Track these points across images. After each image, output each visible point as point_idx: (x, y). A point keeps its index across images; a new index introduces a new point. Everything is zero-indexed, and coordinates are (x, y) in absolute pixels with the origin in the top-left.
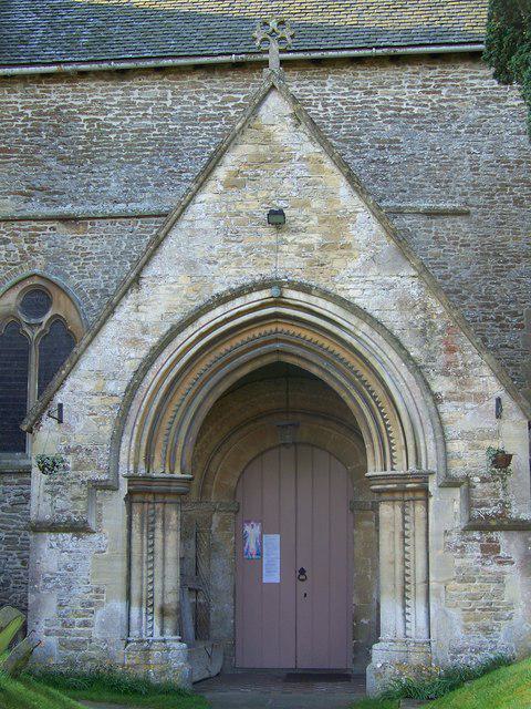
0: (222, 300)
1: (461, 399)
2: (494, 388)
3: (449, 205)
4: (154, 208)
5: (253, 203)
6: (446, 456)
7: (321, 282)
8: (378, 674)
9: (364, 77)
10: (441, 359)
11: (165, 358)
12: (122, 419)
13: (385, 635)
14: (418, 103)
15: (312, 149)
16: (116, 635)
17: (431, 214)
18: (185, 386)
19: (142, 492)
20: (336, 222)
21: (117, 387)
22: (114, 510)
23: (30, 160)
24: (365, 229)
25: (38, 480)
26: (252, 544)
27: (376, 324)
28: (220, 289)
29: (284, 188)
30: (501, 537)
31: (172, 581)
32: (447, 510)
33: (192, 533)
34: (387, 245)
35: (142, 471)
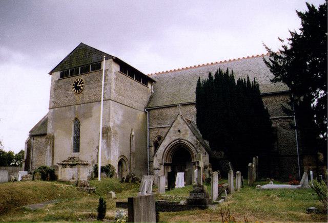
11: (167, 148)
12: (163, 156)
27: (191, 143)
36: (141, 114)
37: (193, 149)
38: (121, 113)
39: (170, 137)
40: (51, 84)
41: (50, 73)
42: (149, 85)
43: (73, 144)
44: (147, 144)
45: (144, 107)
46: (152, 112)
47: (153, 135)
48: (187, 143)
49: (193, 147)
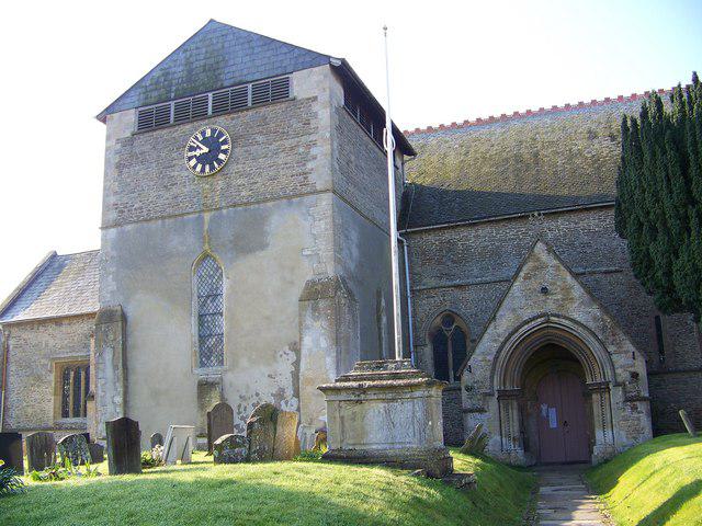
0: (527, 322)
1: (620, 353)
2: (632, 348)
3: (613, 269)
4: (493, 279)
5: (535, 284)
6: (615, 374)
7: (563, 313)
8: (596, 456)
9: (574, 217)
10: (611, 339)
11: (508, 346)
12: (493, 369)
13: (598, 442)
14: (597, 226)
15: (556, 262)
16: (497, 448)
17: (606, 272)
18: (518, 351)
19: (503, 396)
20: (567, 290)
21: (491, 358)
22: (493, 404)
23: (440, 262)
24: (578, 291)
25: (464, 394)
26: (544, 413)
27: (585, 327)
29: (547, 277)
30: (638, 403)
31: (516, 428)
32: (617, 395)
33: (521, 410)
34: (586, 297)
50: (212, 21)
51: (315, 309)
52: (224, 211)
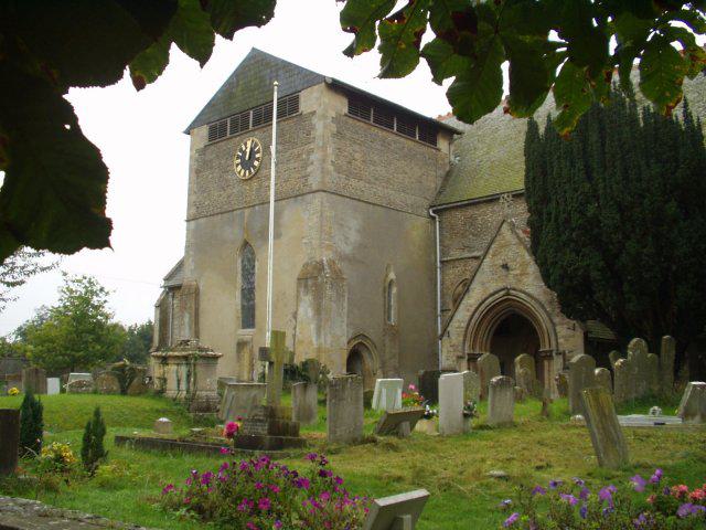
6: (557, 346)
11: (477, 315)
12: (465, 336)
18: (483, 327)
27: (536, 300)
28: (492, 291)
35: (472, 352)
36: (417, 227)
37: (542, 316)
38: (354, 224)
39: (483, 284)
40: (191, 157)
41: (188, 132)
42: (442, 144)
43: (239, 307)
44: (436, 303)
45: (426, 203)
46: (447, 215)
47: (448, 278)
48: (529, 300)
49: (541, 310)
50: (345, 30)
51: (306, 286)
52: (257, 208)
